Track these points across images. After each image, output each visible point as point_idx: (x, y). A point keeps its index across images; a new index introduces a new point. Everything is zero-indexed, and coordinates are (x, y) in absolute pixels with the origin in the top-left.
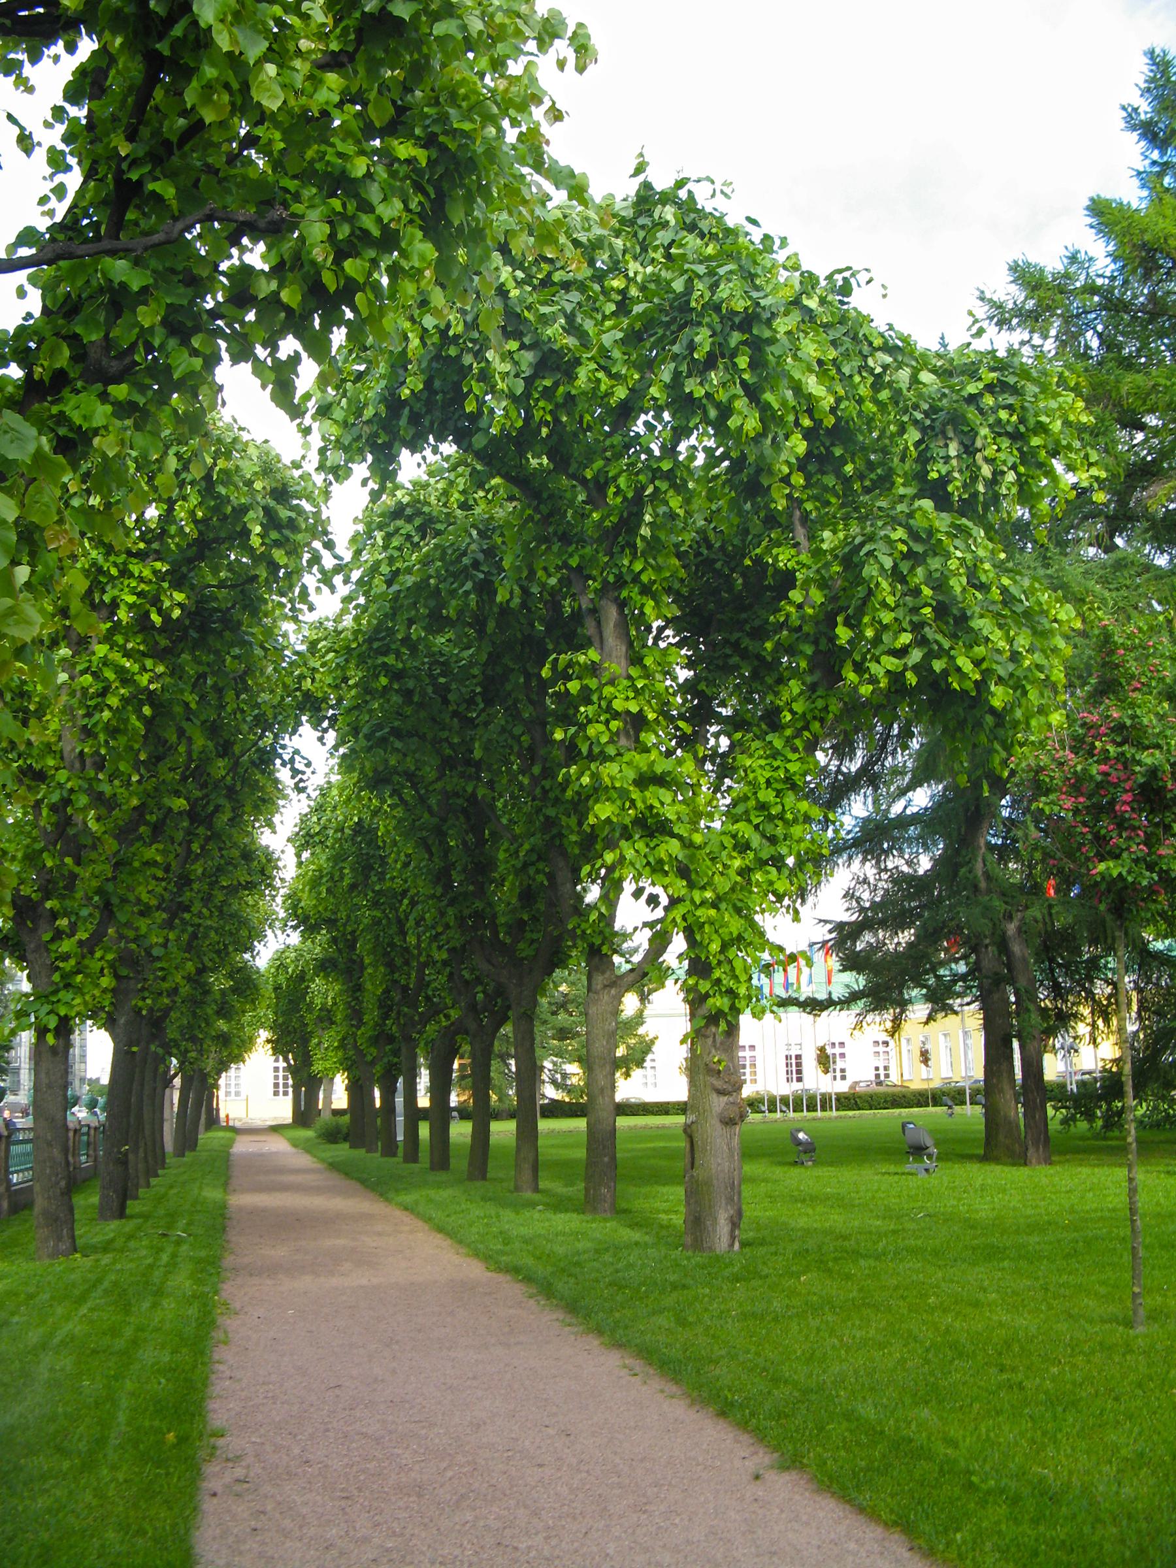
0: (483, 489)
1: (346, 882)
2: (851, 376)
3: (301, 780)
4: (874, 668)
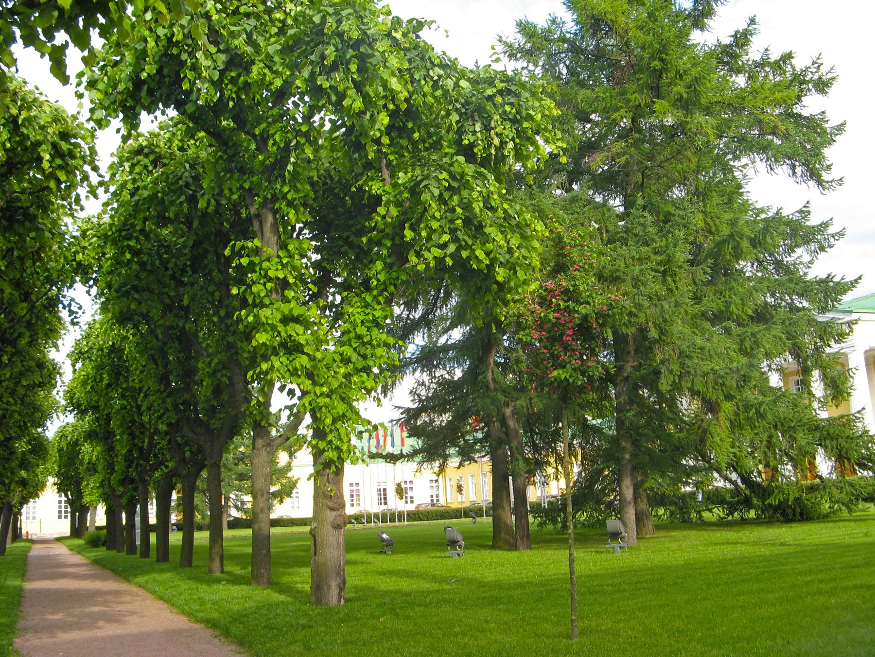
0: (194, 139)
1: (105, 382)
2: (419, 80)
3: (76, 317)
4: (426, 254)
